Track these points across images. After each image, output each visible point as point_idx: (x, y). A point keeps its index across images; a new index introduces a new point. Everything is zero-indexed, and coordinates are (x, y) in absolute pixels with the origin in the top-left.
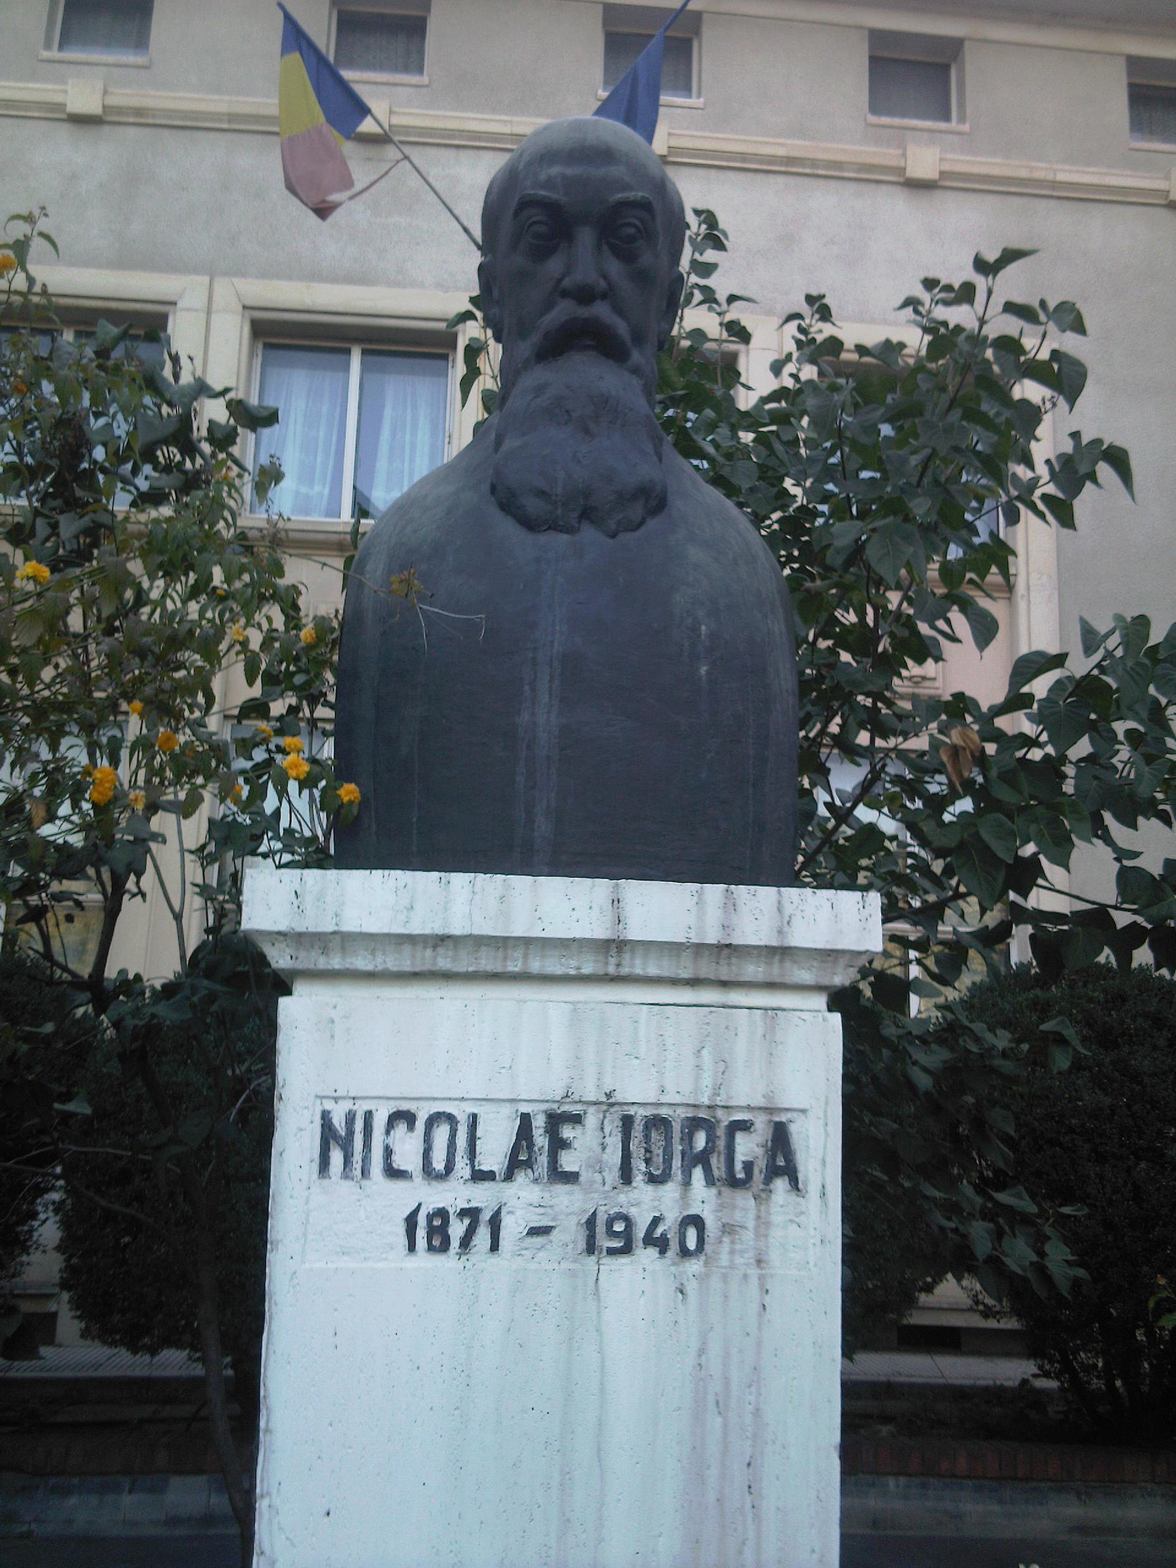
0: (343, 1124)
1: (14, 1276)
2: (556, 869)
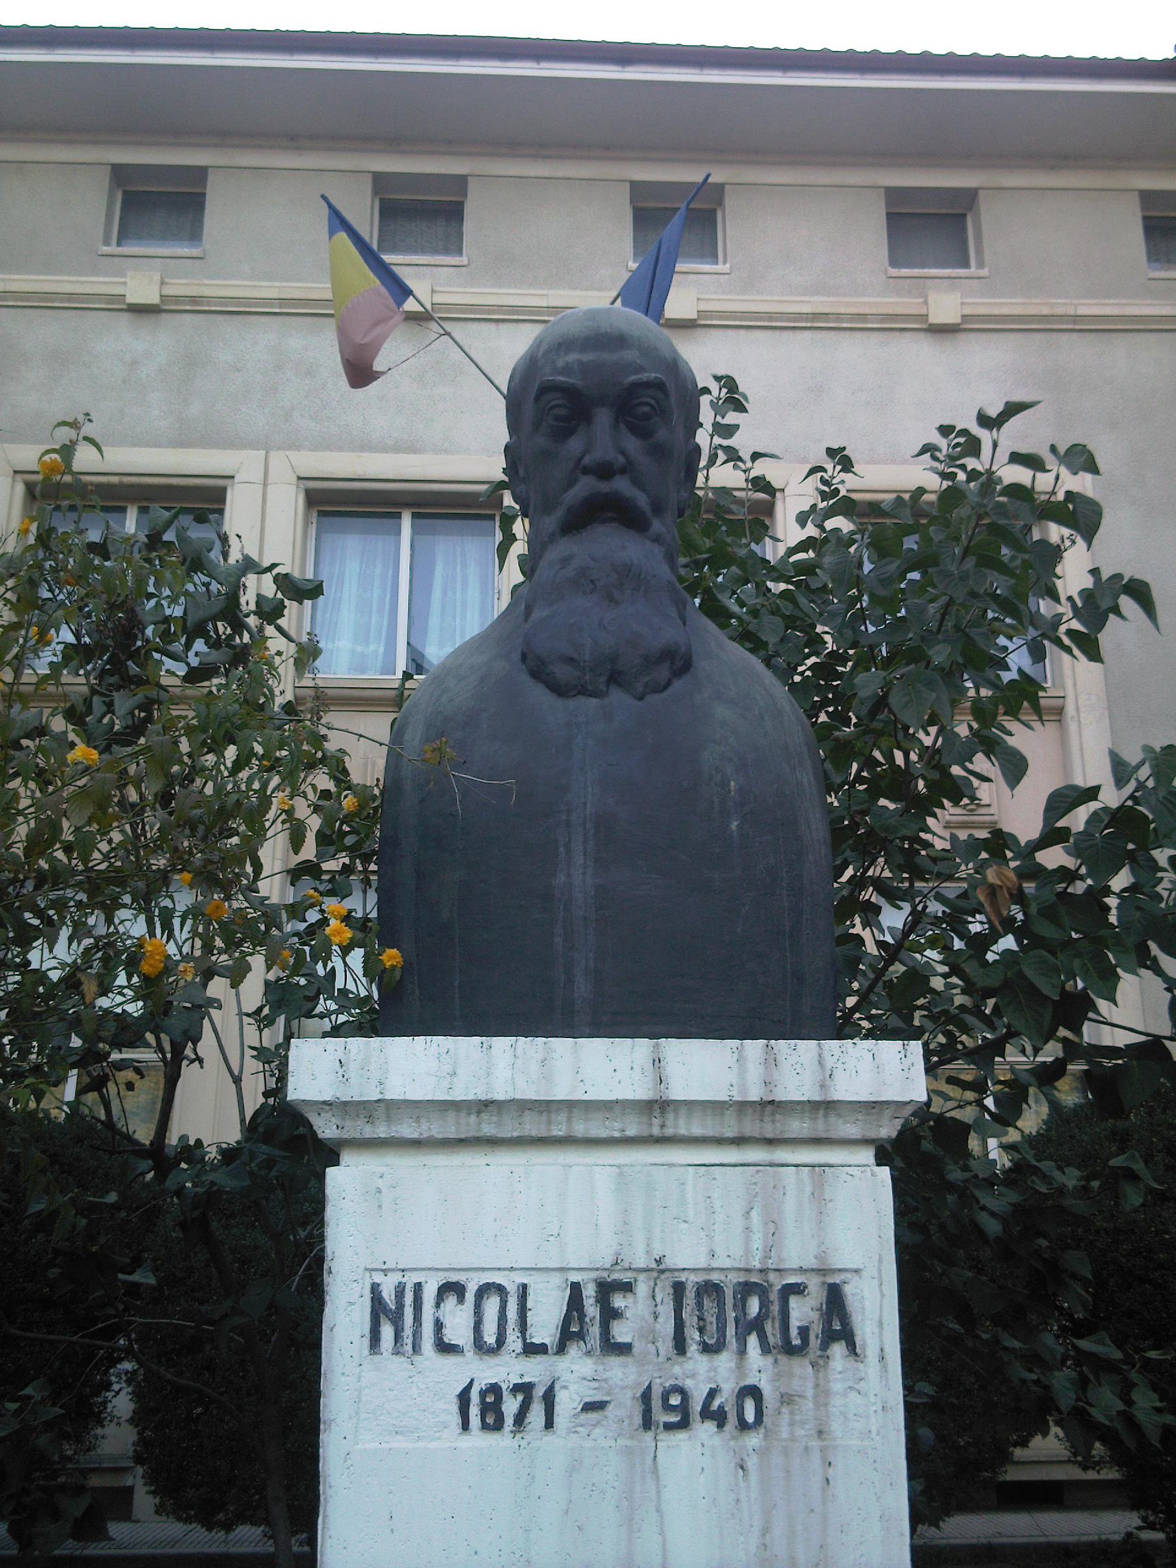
0: (393, 1297)
1: (88, 1450)
2: (598, 1029)
